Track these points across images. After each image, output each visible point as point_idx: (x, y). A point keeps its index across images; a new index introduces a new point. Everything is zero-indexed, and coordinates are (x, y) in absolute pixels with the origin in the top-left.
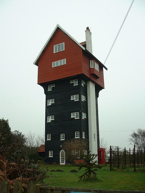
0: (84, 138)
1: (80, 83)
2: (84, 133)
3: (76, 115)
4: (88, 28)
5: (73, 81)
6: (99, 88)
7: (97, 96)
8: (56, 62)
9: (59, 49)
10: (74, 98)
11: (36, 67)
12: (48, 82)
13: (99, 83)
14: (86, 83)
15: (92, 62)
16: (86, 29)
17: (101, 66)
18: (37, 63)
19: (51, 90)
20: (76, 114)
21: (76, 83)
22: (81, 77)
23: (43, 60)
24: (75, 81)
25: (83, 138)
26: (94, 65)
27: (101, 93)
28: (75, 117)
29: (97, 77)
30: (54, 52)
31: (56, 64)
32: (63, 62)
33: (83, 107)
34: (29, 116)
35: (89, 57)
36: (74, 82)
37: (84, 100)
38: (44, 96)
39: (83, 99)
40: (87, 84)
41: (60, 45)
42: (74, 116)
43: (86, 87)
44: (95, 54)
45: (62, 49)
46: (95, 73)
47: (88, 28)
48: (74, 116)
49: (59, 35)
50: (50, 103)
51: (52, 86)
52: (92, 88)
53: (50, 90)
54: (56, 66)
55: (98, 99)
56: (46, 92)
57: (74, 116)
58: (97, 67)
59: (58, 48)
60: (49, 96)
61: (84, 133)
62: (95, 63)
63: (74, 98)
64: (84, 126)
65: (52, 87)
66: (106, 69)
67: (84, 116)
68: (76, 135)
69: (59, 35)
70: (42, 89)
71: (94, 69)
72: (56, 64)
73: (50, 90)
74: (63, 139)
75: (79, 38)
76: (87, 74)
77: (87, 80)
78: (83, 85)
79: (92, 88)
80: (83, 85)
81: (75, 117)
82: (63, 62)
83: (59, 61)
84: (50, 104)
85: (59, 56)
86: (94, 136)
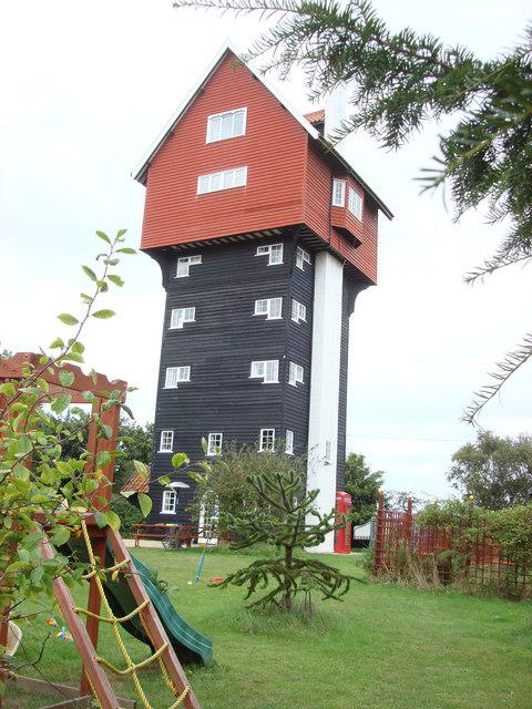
1: (290, 257)
2: (290, 436)
5: (267, 250)
6: (356, 280)
7: (348, 307)
11: (140, 191)
13: (359, 264)
14: (313, 260)
15: (339, 186)
17: (372, 204)
18: (143, 177)
22: (294, 236)
24: (274, 248)
26: (346, 202)
27: (364, 298)
29: (352, 241)
31: (209, 183)
32: (236, 178)
33: (295, 343)
36: (270, 252)
37: (300, 320)
38: (162, 295)
39: (298, 313)
43: (311, 271)
48: (265, 371)
50: (183, 317)
52: (330, 277)
54: (269, 300)
56: (169, 281)
58: (356, 205)
59: (225, 126)
60: (177, 293)
61: (290, 436)
62: (351, 191)
63: (269, 309)
64: (291, 409)
65: (190, 263)
66: (390, 215)
67: (296, 375)
70: (153, 269)
76: (322, 231)
77: (316, 248)
78: (300, 265)
79: (330, 277)
80: (300, 265)
82: (236, 178)
84: (170, 384)
85: (225, 155)
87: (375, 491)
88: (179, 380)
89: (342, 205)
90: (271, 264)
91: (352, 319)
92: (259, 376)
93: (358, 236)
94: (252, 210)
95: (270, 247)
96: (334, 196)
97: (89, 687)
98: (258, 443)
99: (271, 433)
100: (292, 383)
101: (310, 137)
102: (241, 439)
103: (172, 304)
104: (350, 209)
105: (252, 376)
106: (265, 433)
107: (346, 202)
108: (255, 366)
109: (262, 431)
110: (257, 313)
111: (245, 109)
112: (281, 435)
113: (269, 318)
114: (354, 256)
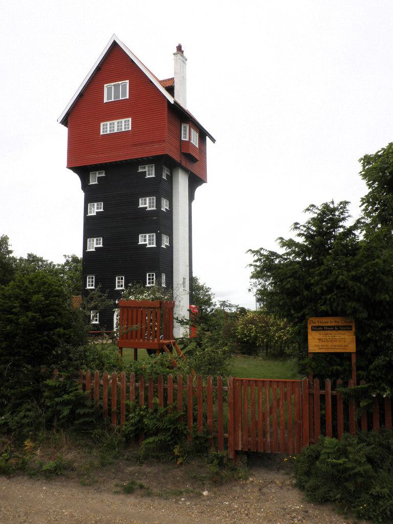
0: (164, 285)
1: (159, 172)
2: (164, 277)
3: (150, 240)
4: (179, 48)
5: (144, 168)
6: (196, 181)
7: (191, 197)
8: (108, 123)
9: (117, 95)
10: (146, 203)
11: (65, 130)
12: (90, 165)
14: (171, 173)
16: (175, 50)
17: (203, 134)
18: (65, 122)
19: (97, 183)
20: (149, 236)
21: (150, 173)
23: (82, 115)
24: (149, 167)
25: (162, 246)
26: (190, 138)
27: (200, 191)
28: (147, 242)
29: (192, 159)
30: (105, 100)
31: (109, 127)
32: (123, 125)
33: (162, 223)
34: (51, 226)
35: (180, 116)
36: (146, 169)
37: (166, 209)
38: (81, 195)
39: (165, 206)
40: (173, 173)
41: (119, 85)
42: (145, 204)
43: (170, 179)
44: (191, 106)
45: (124, 95)
46: (191, 153)
47: (179, 48)
48: (146, 240)
49: (116, 62)
50: (96, 209)
51: (99, 173)
52: (182, 182)
53: (93, 181)
54: (108, 132)
55: (192, 204)
56: (85, 186)
57: (146, 240)
58: (195, 140)
59: (116, 91)
60: (91, 195)
61: (164, 277)
62: (192, 130)
63: (146, 203)
64: (162, 261)
65: (98, 175)
66: (213, 140)
67: (165, 243)
68: (149, 279)
69: (116, 62)
71: (189, 142)
72: (109, 127)
73: (93, 181)
74: (92, 286)
75: (157, 66)
76: (176, 157)
78: (164, 177)
79: (182, 182)
80: (164, 177)
81: (147, 242)
82: (123, 125)
83: (116, 122)
84: (91, 249)
85: (116, 110)
86: (184, 283)
87: (210, 299)
88: (95, 246)
89: (187, 139)
90: (147, 177)
91: (193, 203)
92: (143, 243)
93: (197, 157)
94: (136, 145)
95: (147, 166)
96: (182, 130)
97: (332, 399)
98: (146, 282)
99: (153, 275)
100: (163, 246)
101: (168, 101)
102: (136, 279)
103: (89, 200)
104: (192, 142)
105: (140, 243)
106: (149, 275)
107: (190, 138)
108: (140, 237)
109: (130, 129)
110: (141, 206)
111: (128, 81)
112: (159, 277)
113: (148, 246)
114: (195, 168)
